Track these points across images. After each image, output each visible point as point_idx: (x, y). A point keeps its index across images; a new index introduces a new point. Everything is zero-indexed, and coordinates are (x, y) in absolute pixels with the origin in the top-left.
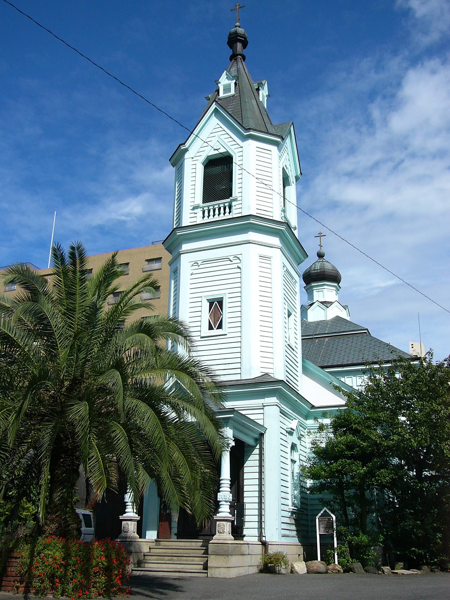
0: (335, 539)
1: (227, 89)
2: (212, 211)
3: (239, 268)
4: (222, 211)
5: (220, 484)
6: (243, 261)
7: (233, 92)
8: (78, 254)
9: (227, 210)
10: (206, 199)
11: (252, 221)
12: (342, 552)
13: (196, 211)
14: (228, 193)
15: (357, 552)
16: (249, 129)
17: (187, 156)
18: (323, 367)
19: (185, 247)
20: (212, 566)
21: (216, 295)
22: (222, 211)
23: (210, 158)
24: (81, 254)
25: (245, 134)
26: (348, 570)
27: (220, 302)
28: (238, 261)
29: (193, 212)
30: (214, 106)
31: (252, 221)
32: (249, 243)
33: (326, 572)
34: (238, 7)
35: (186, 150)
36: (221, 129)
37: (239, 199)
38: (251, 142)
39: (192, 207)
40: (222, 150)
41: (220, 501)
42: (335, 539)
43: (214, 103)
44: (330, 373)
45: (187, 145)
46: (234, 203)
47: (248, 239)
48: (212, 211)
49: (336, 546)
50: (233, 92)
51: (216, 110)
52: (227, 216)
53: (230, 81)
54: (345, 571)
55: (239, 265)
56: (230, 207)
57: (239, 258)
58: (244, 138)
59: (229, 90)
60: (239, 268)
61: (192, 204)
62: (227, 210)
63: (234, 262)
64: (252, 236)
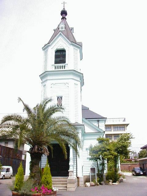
0: (52, 154)
3: (68, 87)
4: (62, 67)
5: (69, 160)
9: (64, 67)
10: (56, 62)
13: (53, 66)
14: (64, 61)
18: (86, 119)
20: (69, 187)
21: (60, 95)
22: (62, 67)
27: (61, 98)
40: (63, 48)
42: (52, 154)
44: (88, 121)
45: (50, 44)
46: (66, 65)
52: (64, 69)
56: (65, 66)
60: (68, 87)
62: (64, 67)
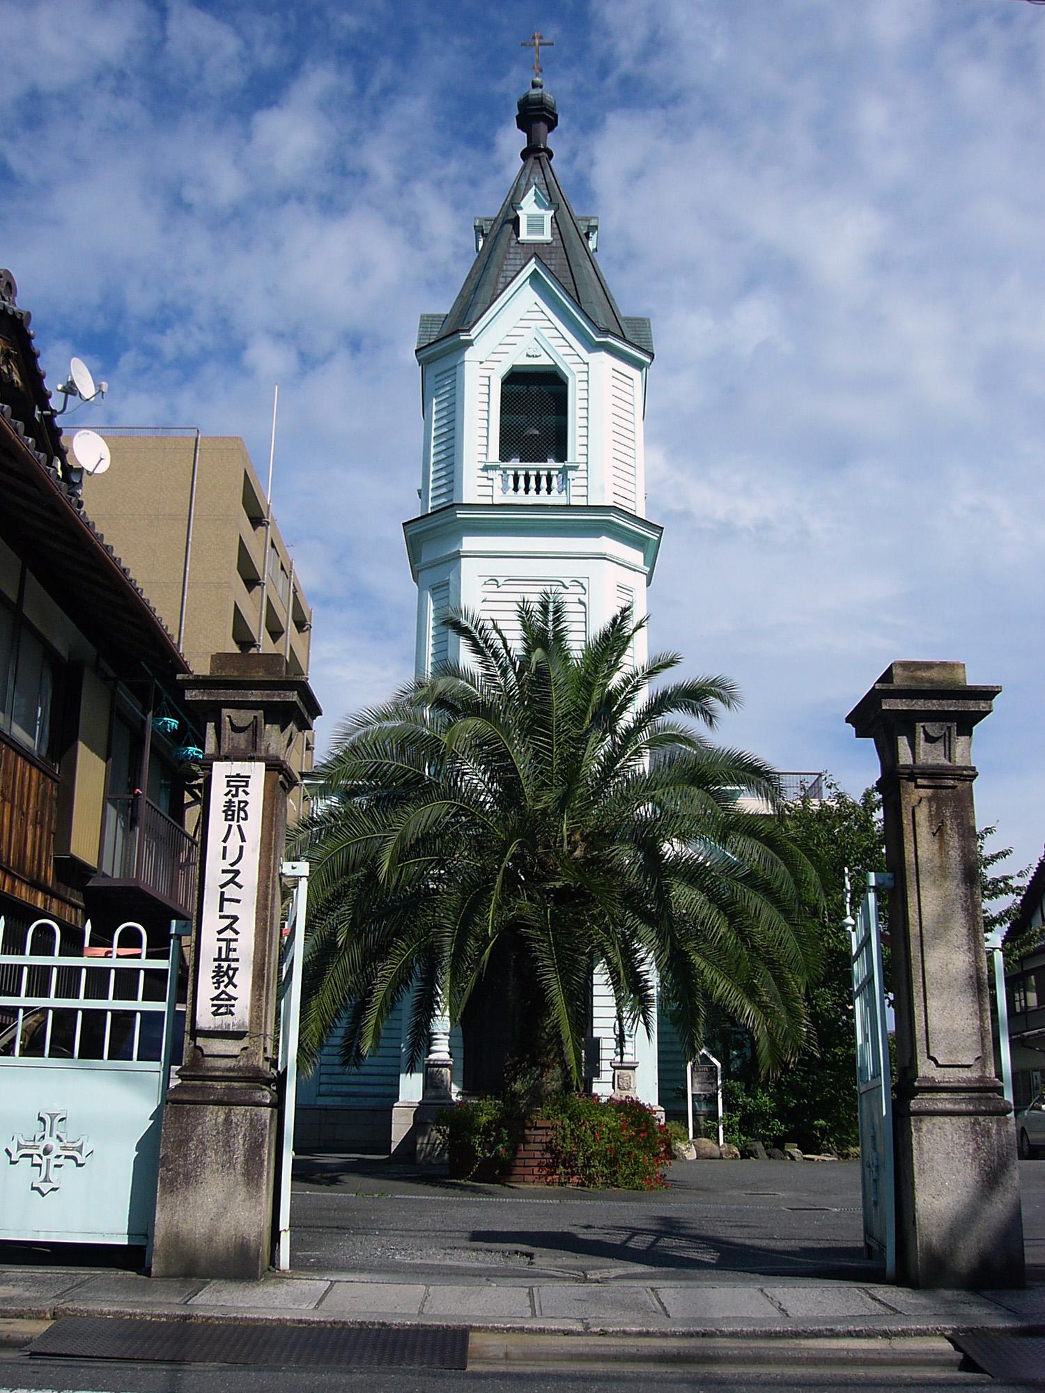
1: (535, 226)
2: (533, 480)
6: (592, 592)
7: (547, 236)
8: (552, 609)
11: (613, 518)
12: (730, 1126)
13: (491, 474)
15: (748, 1123)
16: (606, 332)
17: (469, 354)
19: (469, 543)
23: (516, 370)
24: (557, 610)
25: (598, 340)
26: (746, 1154)
28: (580, 590)
29: (485, 474)
30: (532, 266)
31: (613, 518)
32: (603, 557)
33: (721, 1158)
34: (537, 41)
35: (469, 343)
36: (542, 316)
37: (582, 467)
38: (603, 356)
39: (482, 466)
40: (544, 361)
41: (598, 1040)
43: (534, 260)
46: (571, 474)
47: (603, 551)
48: (533, 480)
49: (720, 1114)
50: (547, 236)
51: (534, 276)
53: (542, 211)
54: (743, 1156)
55: (583, 598)
56: (565, 479)
57: (582, 585)
58: (593, 347)
59: (541, 230)
61: (483, 458)
63: (571, 590)
64: (605, 544)
